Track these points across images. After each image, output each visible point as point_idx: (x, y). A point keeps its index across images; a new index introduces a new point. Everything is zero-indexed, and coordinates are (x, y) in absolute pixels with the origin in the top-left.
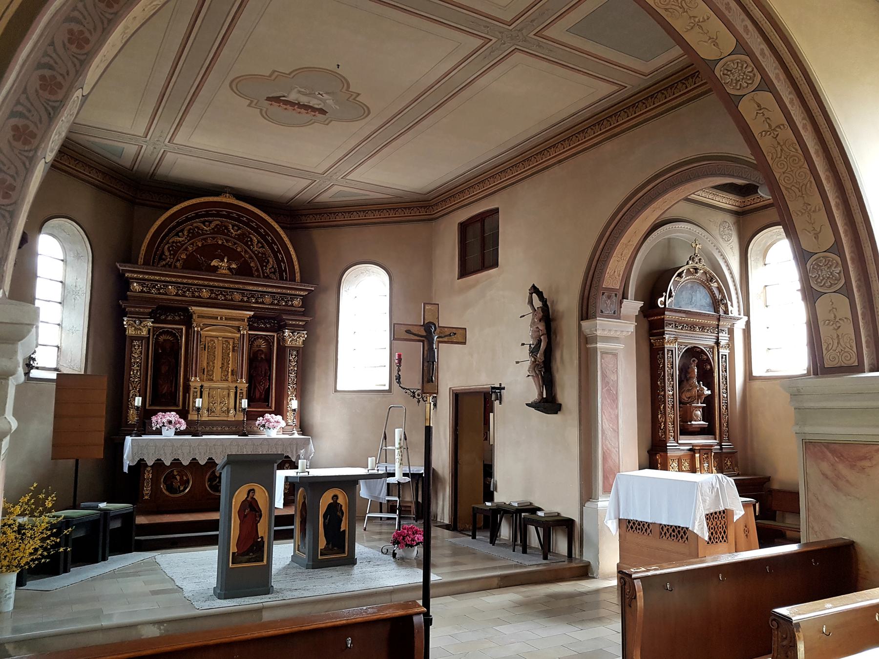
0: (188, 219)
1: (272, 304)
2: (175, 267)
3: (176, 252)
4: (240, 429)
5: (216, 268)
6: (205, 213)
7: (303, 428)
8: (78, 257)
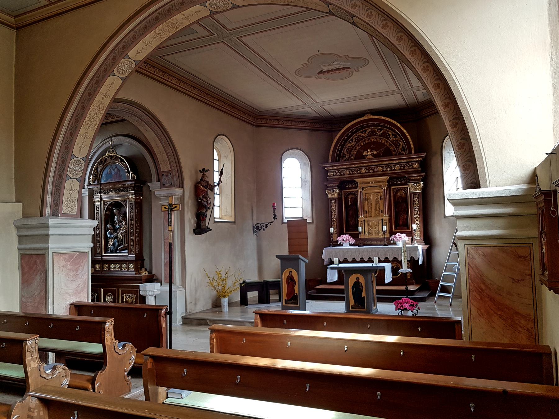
1: (400, 169)
2: (352, 159)
4: (387, 242)
6: (362, 126)
7: (428, 239)
8: (305, 165)
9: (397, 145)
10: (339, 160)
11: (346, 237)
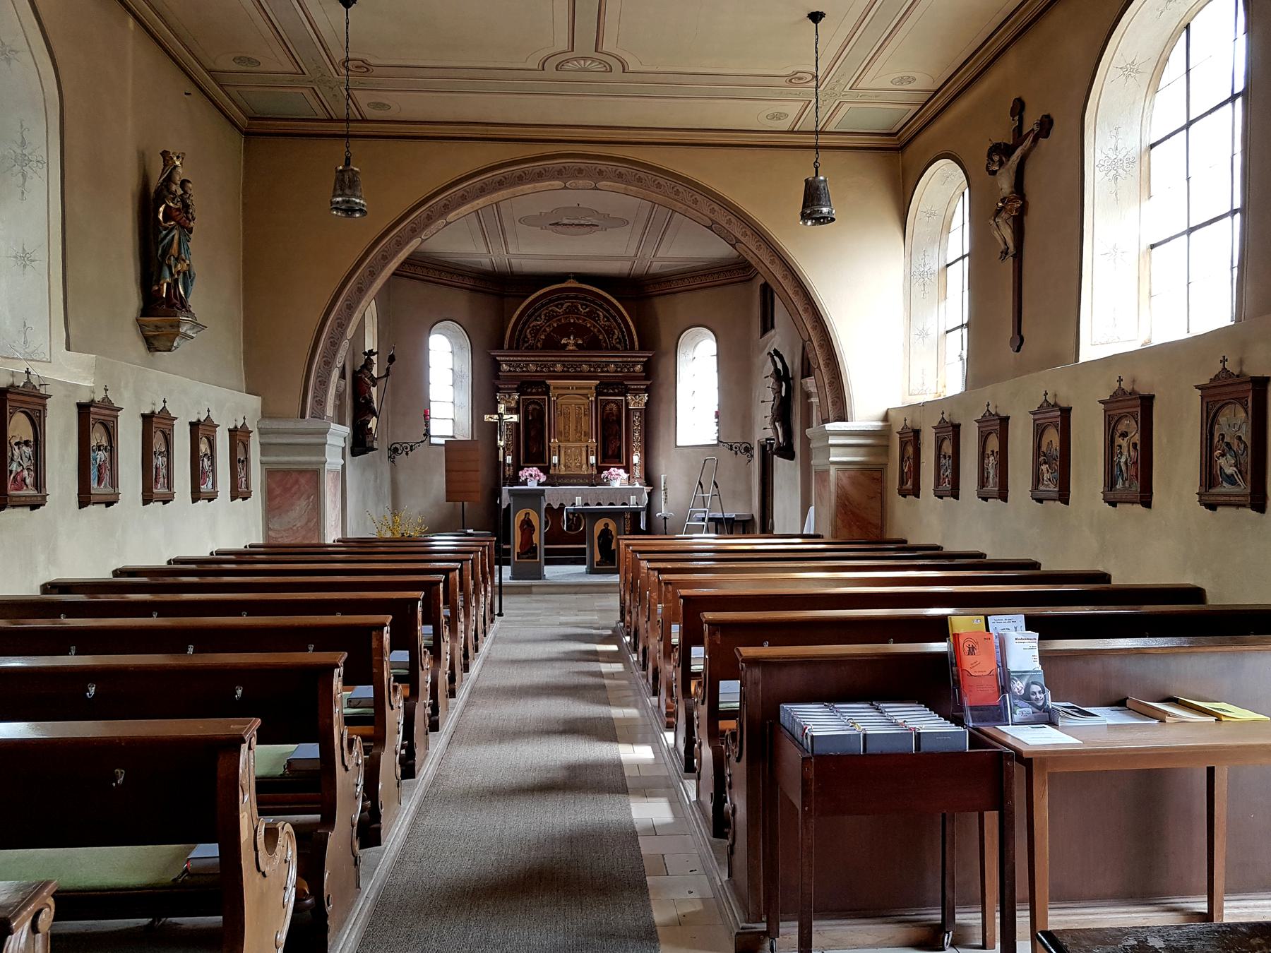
0: (543, 305)
3: (536, 334)
5: (566, 345)
7: (649, 479)
8: (461, 348)
9: (609, 332)
10: (517, 348)
11: (534, 471)
